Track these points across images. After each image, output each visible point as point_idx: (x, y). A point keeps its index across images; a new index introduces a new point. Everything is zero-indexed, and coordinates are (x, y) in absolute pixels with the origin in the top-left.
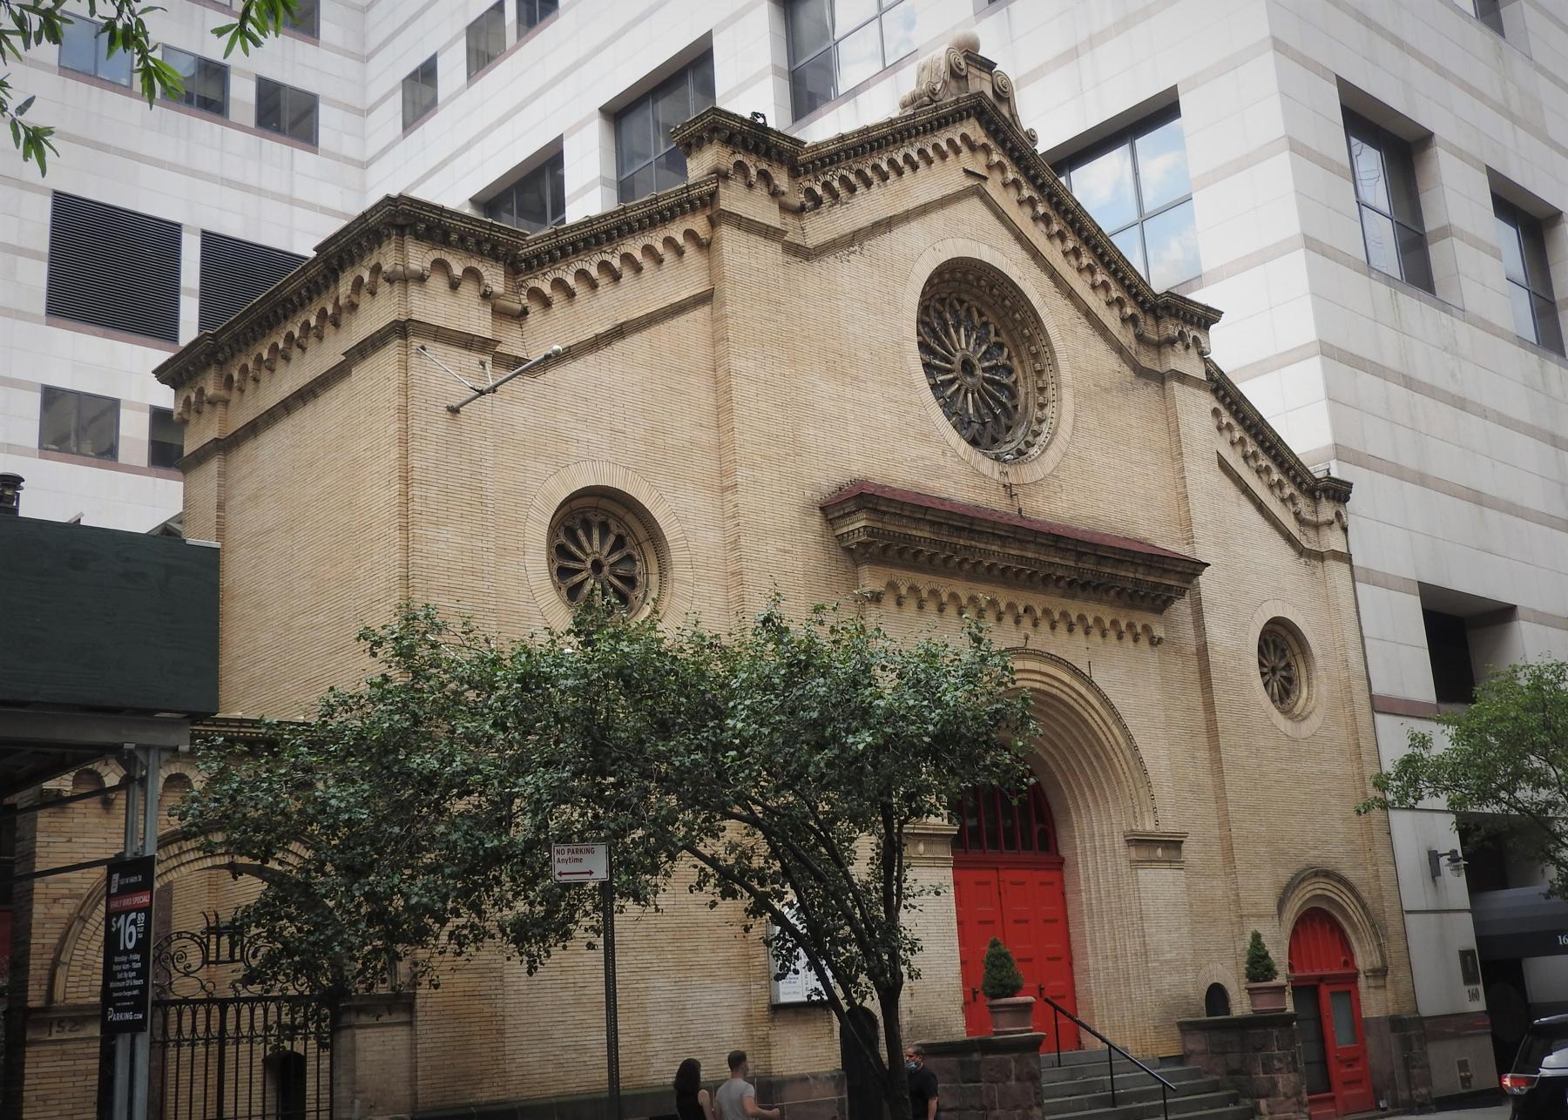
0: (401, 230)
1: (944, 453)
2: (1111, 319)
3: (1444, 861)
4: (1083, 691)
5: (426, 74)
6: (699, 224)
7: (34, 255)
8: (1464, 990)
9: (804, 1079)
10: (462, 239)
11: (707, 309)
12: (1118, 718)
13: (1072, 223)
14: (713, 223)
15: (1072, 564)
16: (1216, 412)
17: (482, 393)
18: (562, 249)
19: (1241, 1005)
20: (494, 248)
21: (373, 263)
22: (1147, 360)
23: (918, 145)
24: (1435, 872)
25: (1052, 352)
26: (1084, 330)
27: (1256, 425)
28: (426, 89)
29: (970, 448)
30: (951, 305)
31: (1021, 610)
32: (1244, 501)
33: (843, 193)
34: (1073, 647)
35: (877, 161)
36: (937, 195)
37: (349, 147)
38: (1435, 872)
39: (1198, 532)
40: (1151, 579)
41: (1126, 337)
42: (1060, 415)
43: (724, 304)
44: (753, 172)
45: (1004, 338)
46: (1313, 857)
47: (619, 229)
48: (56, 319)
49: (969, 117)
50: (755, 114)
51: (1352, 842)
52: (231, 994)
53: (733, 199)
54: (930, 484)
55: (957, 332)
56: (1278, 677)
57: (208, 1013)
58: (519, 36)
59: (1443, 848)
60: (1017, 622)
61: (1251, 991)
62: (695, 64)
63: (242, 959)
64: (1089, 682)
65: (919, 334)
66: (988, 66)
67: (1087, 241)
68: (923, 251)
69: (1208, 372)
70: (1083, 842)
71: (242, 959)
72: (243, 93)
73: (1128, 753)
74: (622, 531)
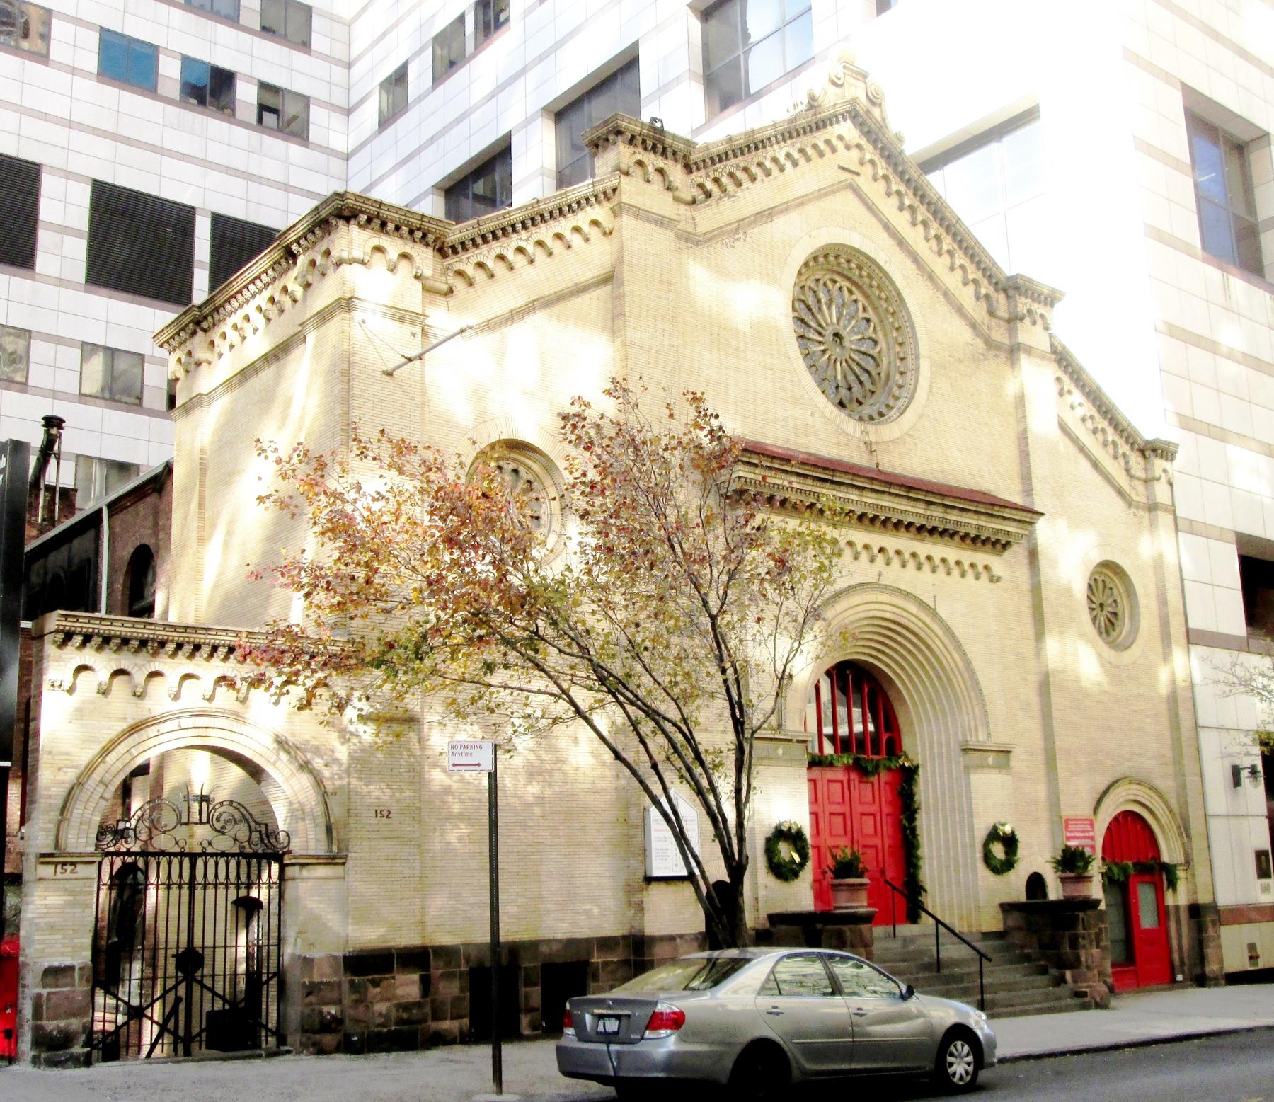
0: (347, 220)
1: (812, 414)
2: (966, 296)
3: (1245, 774)
4: (928, 620)
5: (400, 78)
6: (599, 212)
7: (75, 233)
8: (763, 914)
9: (672, 938)
10: (397, 228)
11: (608, 288)
12: (958, 646)
13: (935, 214)
14: (616, 212)
15: (922, 511)
16: (1058, 379)
17: (410, 360)
18: (504, 230)
19: (1054, 891)
20: (424, 236)
21: (324, 248)
22: (999, 335)
23: (798, 145)
24: (1237, 782)
25: (913, 327)
26: (943, 308)
27: (1094, 392)
28: (398, 90)
29: (836, 410)
30: (825, 284)
31: (876, 550)
32: (1081, 457)
33: (731, 187)
34: (921, 582)
35: (761, 159)
36: (814, 187)
37: (339, 142)
38: (1237, 782)
39: (1036, 485)
40: (992, 526)
41: (977, 311)
42: (917, 381)
43: (622, 284)
44: (651, 169)
45: (870, 314)
46: (1127, 767)
47: (504, 230)
48: (94, 288)
49: (845, 120)
50: (654, 120)
51: (1164, 756)
52: (199, 850)
53: (632, 190)
54: (800, 441)
55: (829, 308)
56: (1105, 612)
57: (238, 864)
58: (476, 47)
59: (1246, 762)
60: (872, 560)
61: (1063, 880)
62: (624, 69)
63: (208, 822)
64: (933, 613)
65: (794, 310)
66: (863, 76)
67: (948, 229)
68: (801, 236)
69: (1052, 345)
70: (923, 750)
71: (208, 822)
72: (246, 94)
73: (966, 675)
74: (531, 478)
